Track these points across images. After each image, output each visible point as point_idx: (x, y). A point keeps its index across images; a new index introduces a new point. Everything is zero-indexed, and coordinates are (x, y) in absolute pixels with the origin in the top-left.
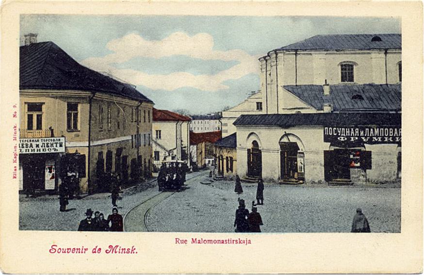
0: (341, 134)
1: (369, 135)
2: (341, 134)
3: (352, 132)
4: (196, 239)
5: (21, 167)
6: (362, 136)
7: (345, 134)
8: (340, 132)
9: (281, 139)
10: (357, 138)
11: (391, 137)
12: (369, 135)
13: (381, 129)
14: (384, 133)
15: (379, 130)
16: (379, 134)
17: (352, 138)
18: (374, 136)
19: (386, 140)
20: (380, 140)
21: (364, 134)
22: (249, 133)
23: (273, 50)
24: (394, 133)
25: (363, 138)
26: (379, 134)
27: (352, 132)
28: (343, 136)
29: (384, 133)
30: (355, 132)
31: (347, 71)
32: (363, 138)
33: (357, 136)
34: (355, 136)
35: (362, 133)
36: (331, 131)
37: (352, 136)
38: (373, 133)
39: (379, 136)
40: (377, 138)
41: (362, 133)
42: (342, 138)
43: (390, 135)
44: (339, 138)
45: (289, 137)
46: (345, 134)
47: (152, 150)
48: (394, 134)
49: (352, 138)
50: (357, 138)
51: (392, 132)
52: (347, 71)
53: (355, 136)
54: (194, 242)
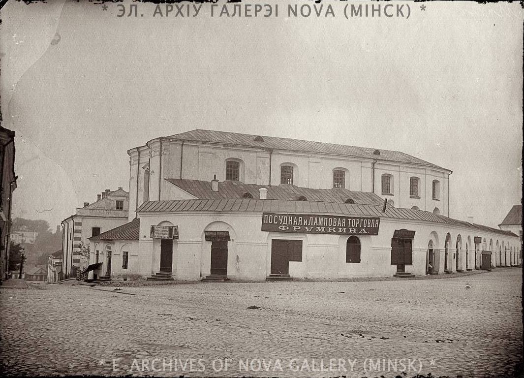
0: (283, 223)
1: (313, 223)
2: (283, 223)
4: (360, 7)
5: (434, 252)
6: (305, 226)
7: (288, 223)
8: (281, 220)
9: (206, 228)
10: (299, 228)
11: (334, 227)
12: (313, 223)
14: (328, 223)
15: (323, 219)
16: (323, 224)
17: (295, 227)
18: (318, 226)
19: (340, 231)
20: (323, 231)
21: (308, 223)
23: (136, 148)
24: (293, 221)
25: (306, 228)
26: (323, 224)
28: (284, 225)
29: (328, 223)
31: (339, 176)
32: (306, 228)
34: (298, 225)
35: (305, 222)
37: (295, 225)
38: (296, 221)
39: (323, 226)
40: (320, 228)
41: (305, 222)
42: (284, 227)
43: (334, 225)
44: (279, 228)
45: (448, 217)
46: (288, 223)
47: (303, 232)
48: (337, 225)
49: (295, 227)
50: (299, 228)
51: (335, 222)
52: (339, 176)
53: (298, 225)
54: (356, 14)
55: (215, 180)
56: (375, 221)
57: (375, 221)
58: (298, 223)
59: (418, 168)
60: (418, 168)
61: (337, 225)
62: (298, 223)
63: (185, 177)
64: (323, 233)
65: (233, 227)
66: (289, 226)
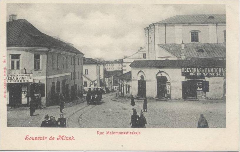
0: (191, 71)
2: (191, 71)
3: (198, 71)
7: (194, 71)
8: (191, 70)
9: (157, 75)
13: (214, 69)
14: (216, 71)
17: (217, 74)
18: (210, 73)
21: (205, 71)
22: (138, 72)
24: (197, 70)
25: (204, 74)
27: (198, 71)
28: (192, 73)
29: (216, 71)
30: (199, 70)
31: (195, 36)
33: (200, 73)
35: (203, 71)
36: (186, 70)
39: (214, 73)
41: (203, 71)
42: (192, 74)
48: (221, 71)
52: (195, 36)
55: (183, 43)
56: (219, 69)
57: (219, 69)
58: (199, 71)
59: (203, 25)
60: (203, 25)
61: (221, 71)
62: (199, 71)
63: (150, 60)
64: (214, 76)
65: (145, 74)
66: (195, 73)
